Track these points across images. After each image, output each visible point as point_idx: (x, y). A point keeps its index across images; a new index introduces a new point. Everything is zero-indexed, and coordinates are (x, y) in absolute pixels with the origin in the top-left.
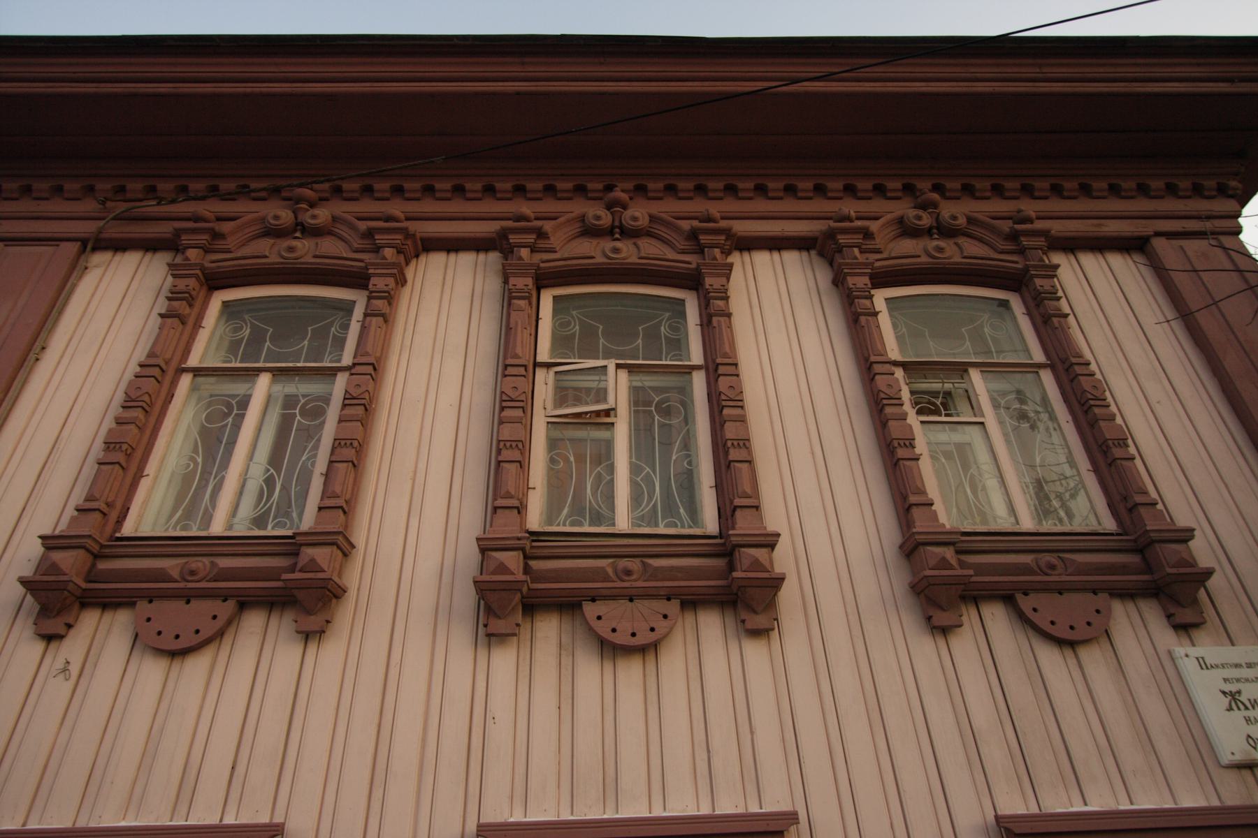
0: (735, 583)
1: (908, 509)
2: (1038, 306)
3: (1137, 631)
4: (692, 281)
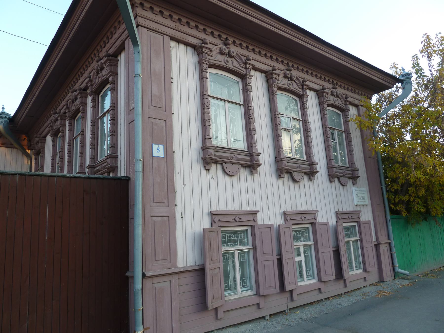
1: (205, 139)
2: (303, 104)
3: (244, 173)
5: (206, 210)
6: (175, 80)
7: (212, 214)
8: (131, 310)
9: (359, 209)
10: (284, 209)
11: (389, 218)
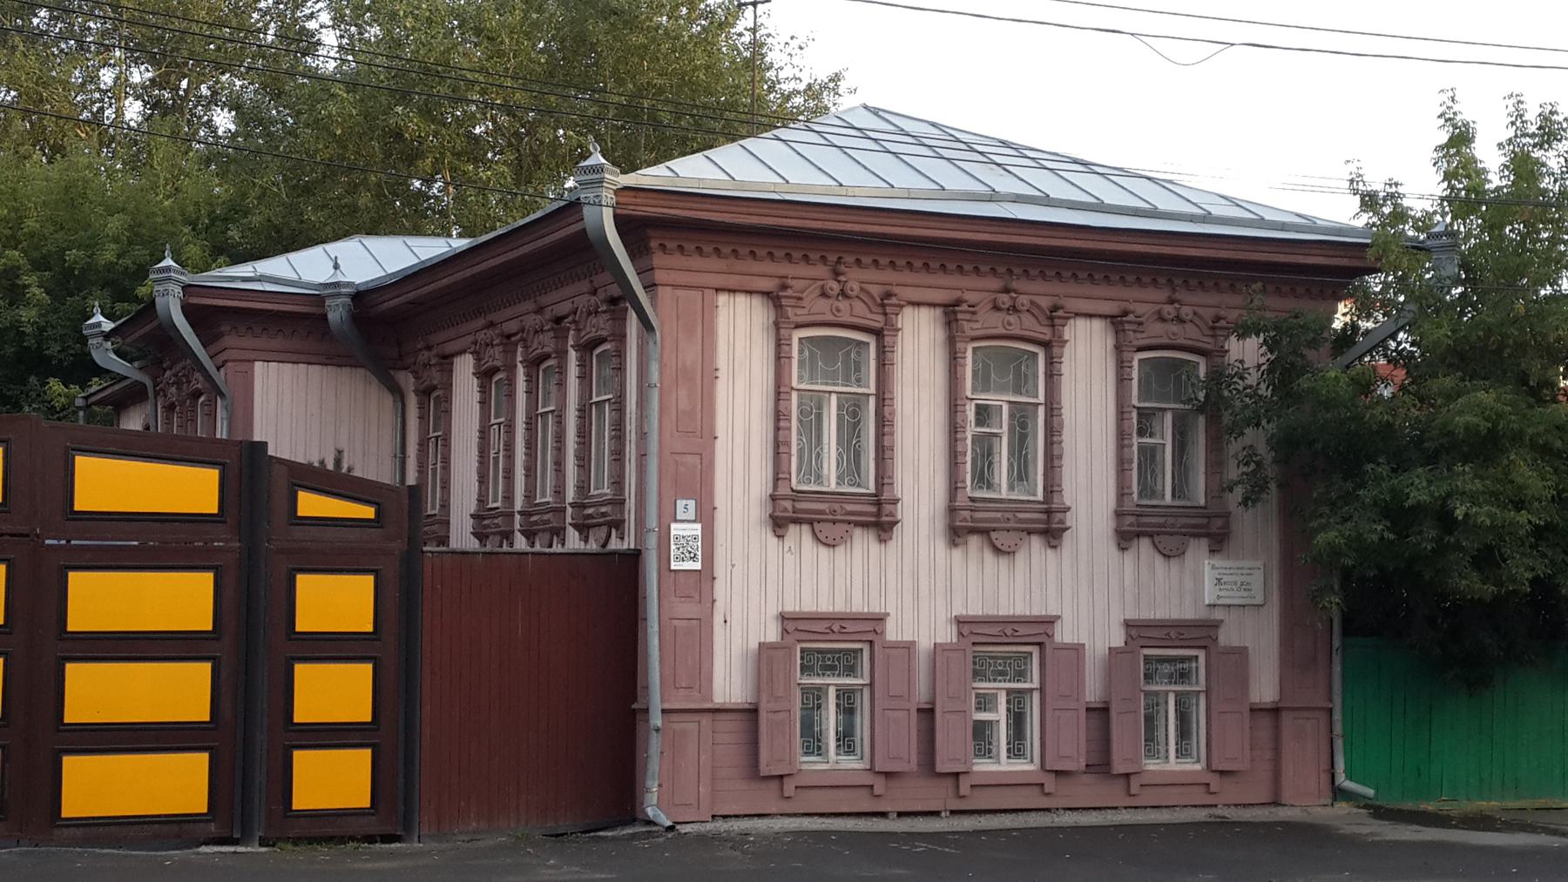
0: (879, 519)
3: (863, 542)
4: (1046, 345)
5: (773, 610)
6: (722, 374)
7: (784, 618)
8: (640, 755)
9: (1218, 615)
10: (959, 610)
11: (1336, 643)
